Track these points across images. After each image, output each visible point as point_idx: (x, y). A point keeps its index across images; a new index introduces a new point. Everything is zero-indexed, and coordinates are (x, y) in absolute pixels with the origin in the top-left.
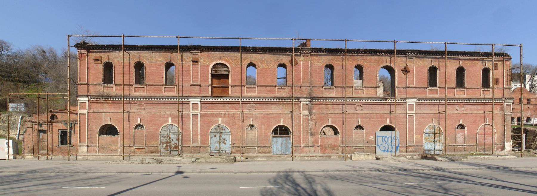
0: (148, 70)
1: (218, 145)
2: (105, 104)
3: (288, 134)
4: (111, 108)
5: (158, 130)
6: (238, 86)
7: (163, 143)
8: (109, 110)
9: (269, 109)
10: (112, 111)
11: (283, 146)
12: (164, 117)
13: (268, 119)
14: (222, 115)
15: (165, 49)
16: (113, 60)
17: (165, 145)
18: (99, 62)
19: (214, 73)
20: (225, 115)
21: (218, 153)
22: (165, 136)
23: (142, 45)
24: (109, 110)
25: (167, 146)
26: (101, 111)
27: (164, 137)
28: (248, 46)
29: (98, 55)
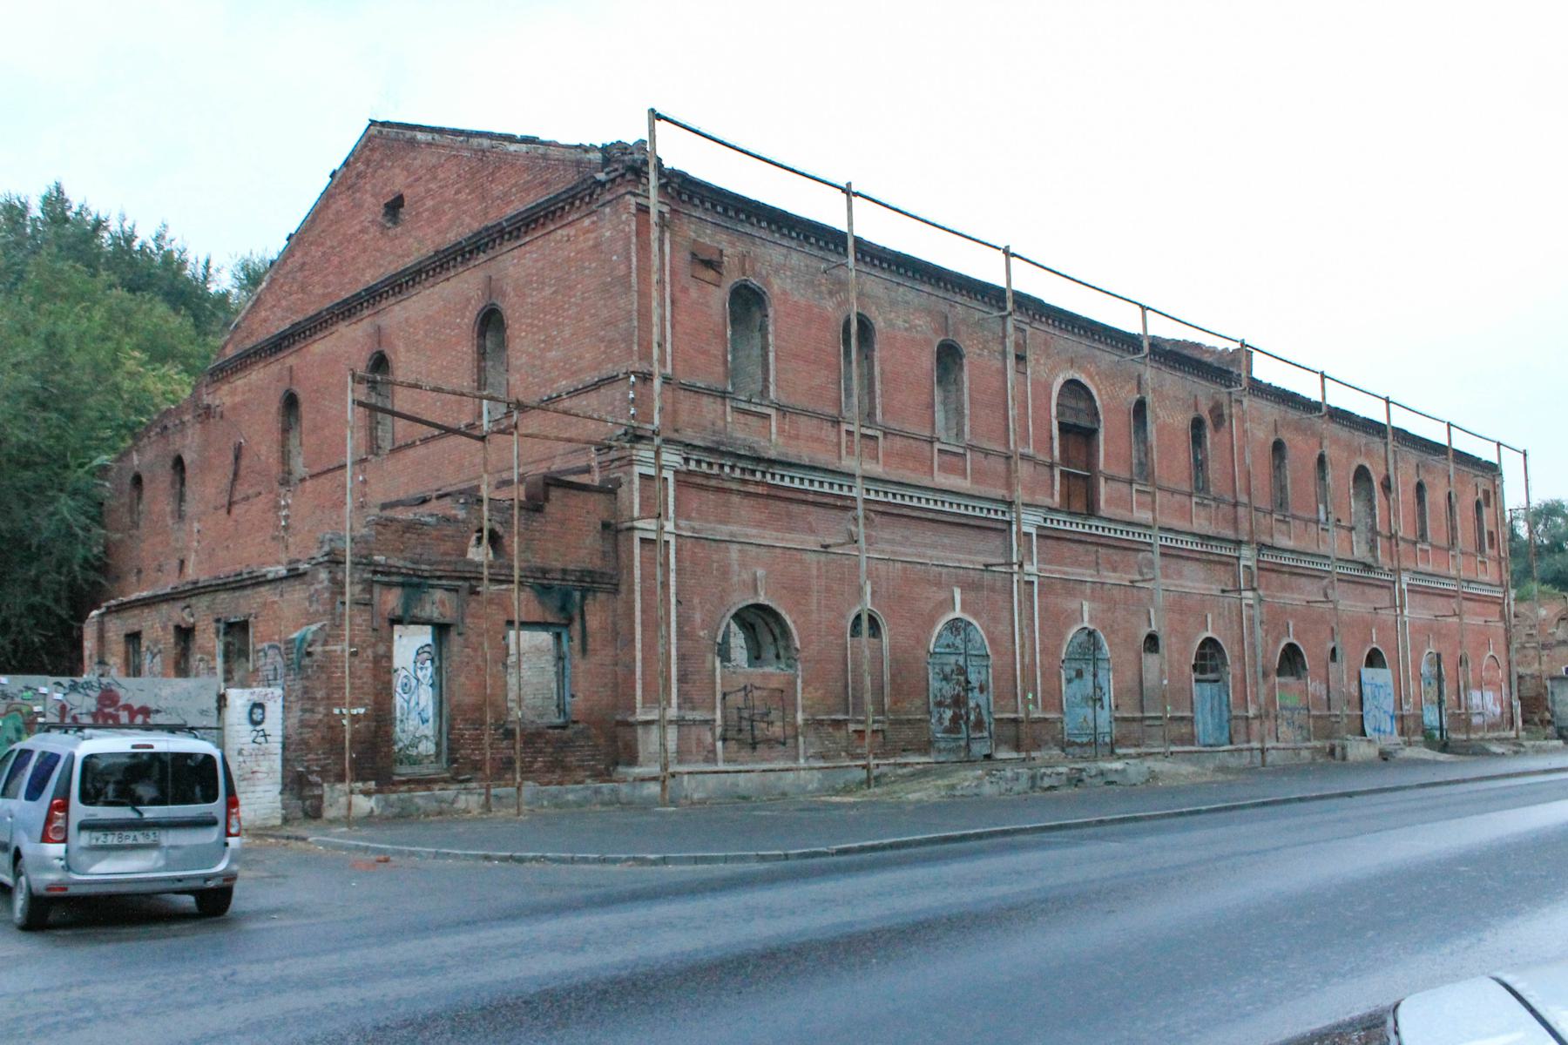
0: (1290, 454)
1: (1090, 711)
2: (735, 499)
3: (1214, 669)
4: (760, 524)
5: (921, 641)
6: (401, 384)
7: (939, 704)
8: (753, 533)
9: (1180, 575)
10: (769, 537)
11: (1216, 712)
12: (938, 584)
13: (1182, 612)
14: (1088, 589)
15: (938, 280)
16: (768, 283)
17: (948, 714)
18: (710, 275)
19: (1071, 420)
20: (1093, 591)
21: (1089, 744)
22: (948, 669)
23: (1477, 455)
24: (753, 533)
25: (955, 719)
26: (723, 531)
27: (946, 678)
28: (1265, 381)
29: (713, 238)
